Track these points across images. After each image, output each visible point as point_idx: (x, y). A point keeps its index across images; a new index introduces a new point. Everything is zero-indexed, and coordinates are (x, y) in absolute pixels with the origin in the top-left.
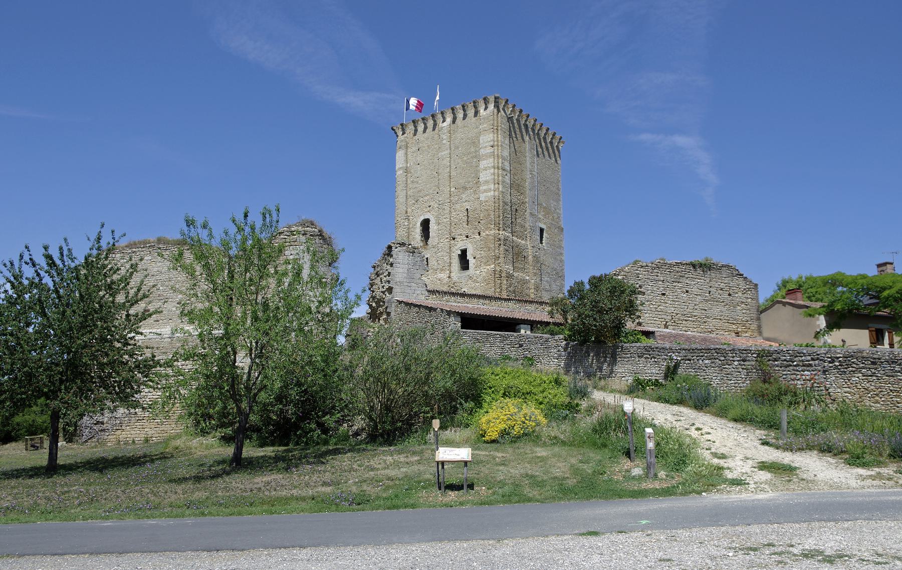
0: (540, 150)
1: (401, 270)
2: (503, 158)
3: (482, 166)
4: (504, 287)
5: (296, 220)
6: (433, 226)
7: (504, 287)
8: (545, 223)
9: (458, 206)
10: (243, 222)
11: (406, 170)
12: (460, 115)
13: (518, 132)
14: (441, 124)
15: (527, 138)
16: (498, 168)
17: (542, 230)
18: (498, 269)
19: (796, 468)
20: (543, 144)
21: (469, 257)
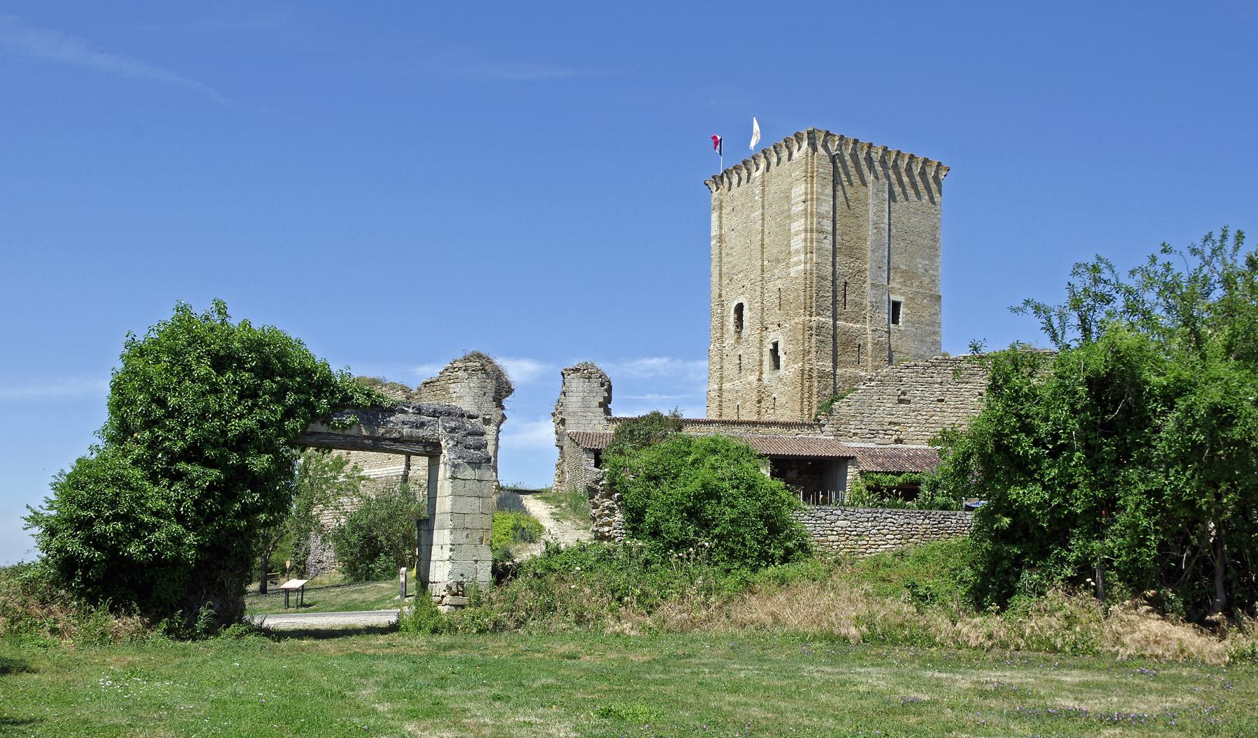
0: (897, 189)
1: (574, 399)
2: (821, 216)
3: (793, 231)
4: (815, 390)
5: (460, 356)
6: (746, 314)
7: (815, 390)
8: (902, 294)
9: (770, 285)
10: (55, 487)
11: (721, 239)
12: (774, 160)
13: (852, 171)
14: (796, 154)
15: (870, 178)
16: (812, 231)
17: (896, 306)
18: (807, 367)
19: (994, 586)
20: (905, 179)
21: (781, 353)
